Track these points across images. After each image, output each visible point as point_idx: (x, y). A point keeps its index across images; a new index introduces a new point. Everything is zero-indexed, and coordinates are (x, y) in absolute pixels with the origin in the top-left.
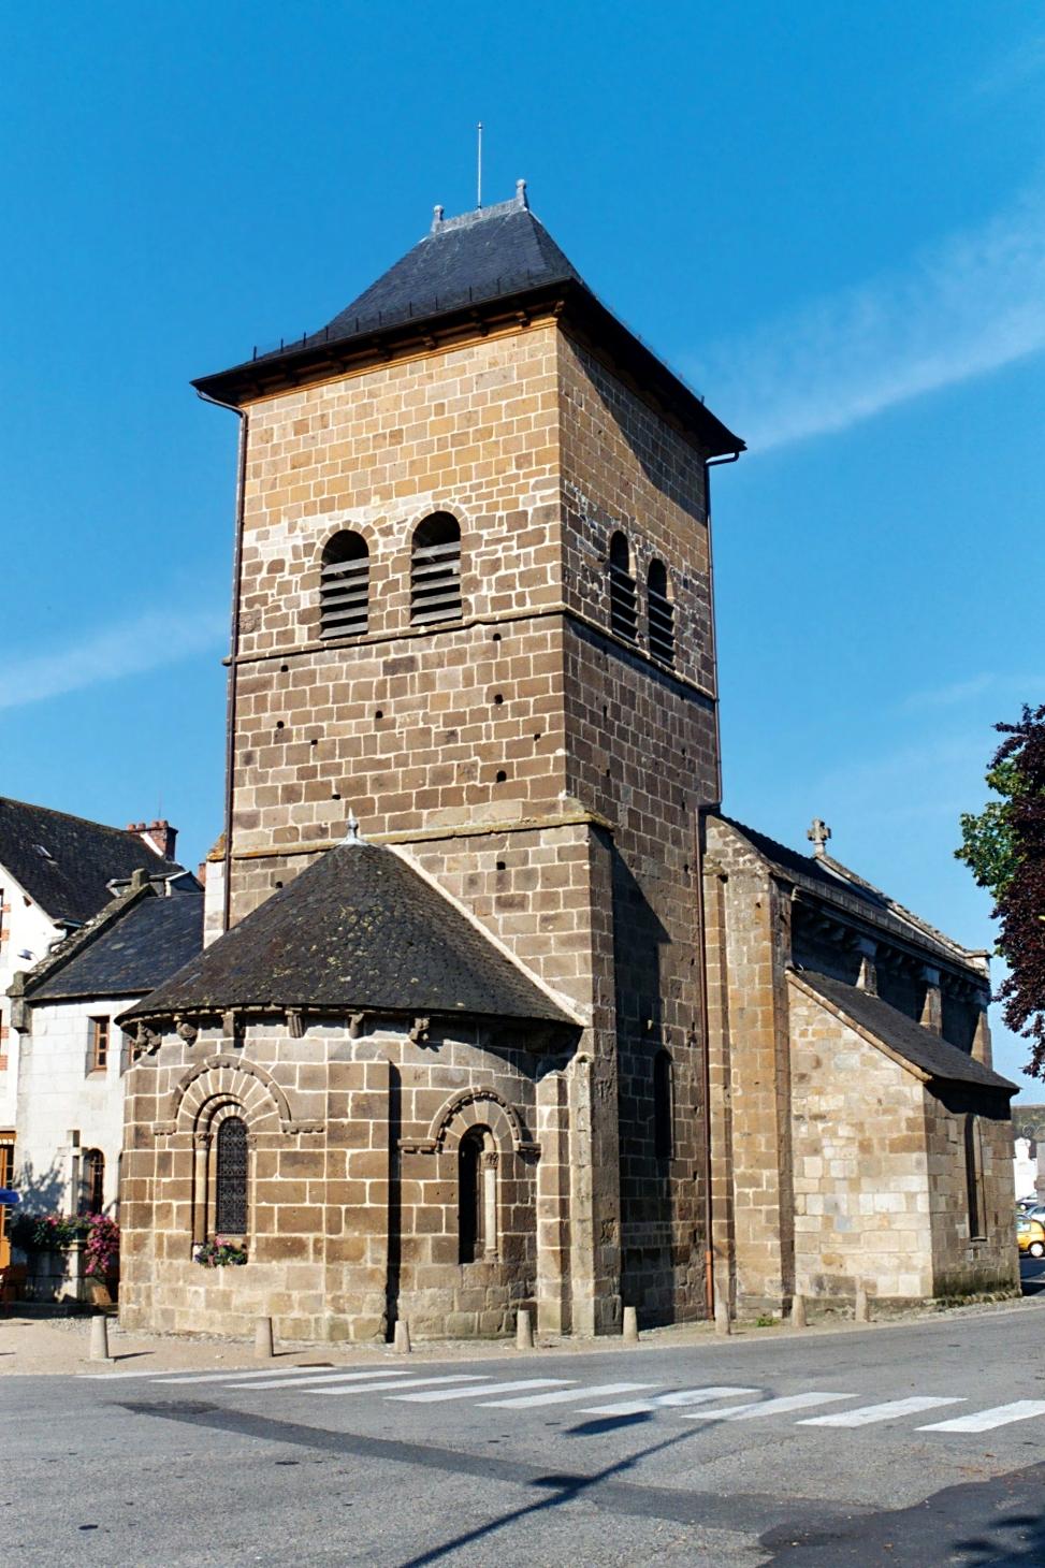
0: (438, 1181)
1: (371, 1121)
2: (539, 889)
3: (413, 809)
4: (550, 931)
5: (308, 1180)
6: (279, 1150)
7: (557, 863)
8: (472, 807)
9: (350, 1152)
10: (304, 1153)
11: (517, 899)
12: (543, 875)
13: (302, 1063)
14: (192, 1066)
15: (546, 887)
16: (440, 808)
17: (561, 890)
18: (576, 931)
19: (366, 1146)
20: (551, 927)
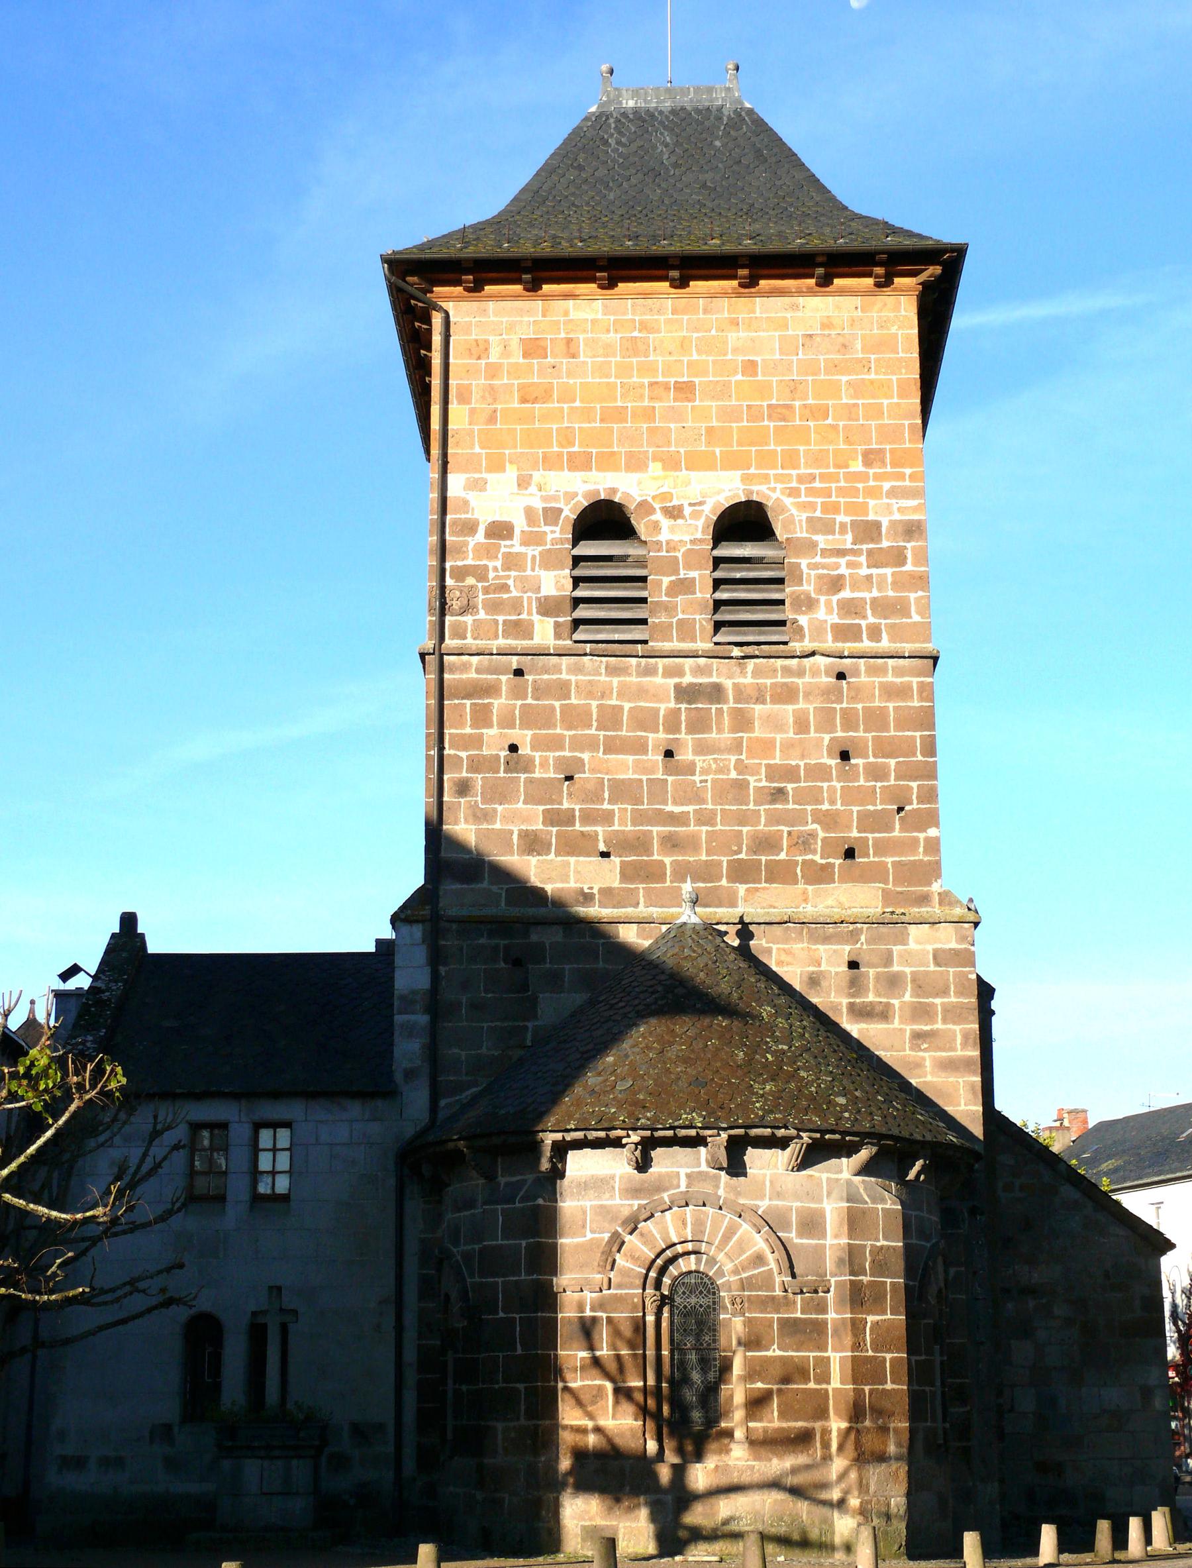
0: (923, 1357)
1: (889, 1280)
2: (908, 997)
3: (724, 882)
4: (925, 1050)
5: (812, 1354)
6: (776, 1316)
7: (932, 968)
8: (810, 888)
9: (871, 1319)
10: (805, 1319)
11: (879, 1009)
12: (913, 981)
13: (799, 1204)
14: (636, 1203)
15: (918, 996)
16: (764, 885)
17: (938, 1001)
18: (959, 1053)
19: (884, 1312)
20: (925, 1046)
